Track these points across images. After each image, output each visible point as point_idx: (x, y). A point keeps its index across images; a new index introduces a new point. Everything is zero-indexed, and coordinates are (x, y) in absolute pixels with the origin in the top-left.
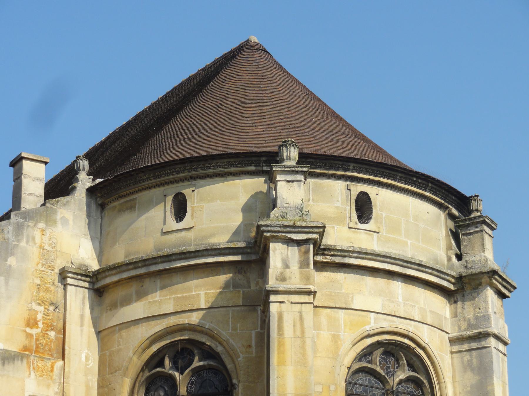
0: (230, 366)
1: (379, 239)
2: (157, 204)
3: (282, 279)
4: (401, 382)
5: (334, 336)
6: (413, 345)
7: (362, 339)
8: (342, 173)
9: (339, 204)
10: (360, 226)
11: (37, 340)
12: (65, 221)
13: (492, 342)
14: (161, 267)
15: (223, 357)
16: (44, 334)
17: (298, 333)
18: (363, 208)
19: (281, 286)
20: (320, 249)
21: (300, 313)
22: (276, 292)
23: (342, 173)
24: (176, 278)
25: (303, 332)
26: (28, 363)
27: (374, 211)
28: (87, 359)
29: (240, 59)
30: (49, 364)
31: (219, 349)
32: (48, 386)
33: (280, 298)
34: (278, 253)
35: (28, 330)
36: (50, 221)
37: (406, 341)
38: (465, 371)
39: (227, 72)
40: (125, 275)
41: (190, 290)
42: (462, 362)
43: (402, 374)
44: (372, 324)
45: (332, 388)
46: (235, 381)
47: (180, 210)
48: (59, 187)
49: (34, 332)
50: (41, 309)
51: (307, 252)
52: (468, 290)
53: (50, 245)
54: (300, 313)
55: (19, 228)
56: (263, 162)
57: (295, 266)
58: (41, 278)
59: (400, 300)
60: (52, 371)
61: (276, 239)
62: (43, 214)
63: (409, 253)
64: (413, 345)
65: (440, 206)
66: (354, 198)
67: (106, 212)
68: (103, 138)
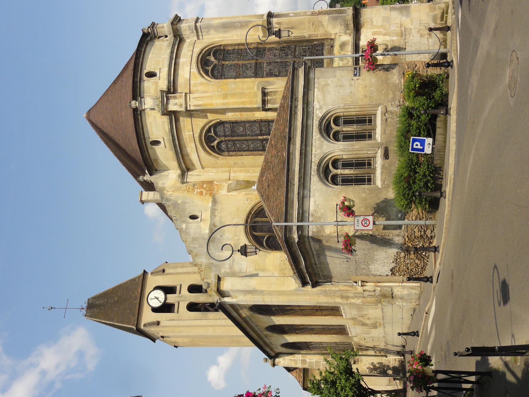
2: (326, 259)
3: (181, 105)
4: (215, 59)
6: (201, 55)
9: (151, 84)
10: (158, 76)
12: (163, 184)
13: (198, 24)
14: (178, 148)
16: (205, 189)
17: (201, 99)
18: (151, 75)
19: (184, 106)
20: (169, 92)
21: (193, 98)
22: (186, 107)
24: (182, 143)
25: (200, 97)
28: (213, 173)
29: (94, 120)
30: (216, 186)
32: (224, 186)
33: (188, 106)
34: (172, 107)
35: (204, 194)
38: (209, 34)
39: (99, 125)
40: (182, 161)
41: (186, 138)
43: (212, 58)
47: (156, 143)
48: (149, 187)
49: (204, 192)
51: (171, 96)
52: (179, 33)
54: (193, 98)
55: (167, 200)
56: (138, 115)
57: (176, 101)
62: (161, 191)
64: (201, 55)
65: (147, 44)
67: (158, 169)
68: (125, 168)
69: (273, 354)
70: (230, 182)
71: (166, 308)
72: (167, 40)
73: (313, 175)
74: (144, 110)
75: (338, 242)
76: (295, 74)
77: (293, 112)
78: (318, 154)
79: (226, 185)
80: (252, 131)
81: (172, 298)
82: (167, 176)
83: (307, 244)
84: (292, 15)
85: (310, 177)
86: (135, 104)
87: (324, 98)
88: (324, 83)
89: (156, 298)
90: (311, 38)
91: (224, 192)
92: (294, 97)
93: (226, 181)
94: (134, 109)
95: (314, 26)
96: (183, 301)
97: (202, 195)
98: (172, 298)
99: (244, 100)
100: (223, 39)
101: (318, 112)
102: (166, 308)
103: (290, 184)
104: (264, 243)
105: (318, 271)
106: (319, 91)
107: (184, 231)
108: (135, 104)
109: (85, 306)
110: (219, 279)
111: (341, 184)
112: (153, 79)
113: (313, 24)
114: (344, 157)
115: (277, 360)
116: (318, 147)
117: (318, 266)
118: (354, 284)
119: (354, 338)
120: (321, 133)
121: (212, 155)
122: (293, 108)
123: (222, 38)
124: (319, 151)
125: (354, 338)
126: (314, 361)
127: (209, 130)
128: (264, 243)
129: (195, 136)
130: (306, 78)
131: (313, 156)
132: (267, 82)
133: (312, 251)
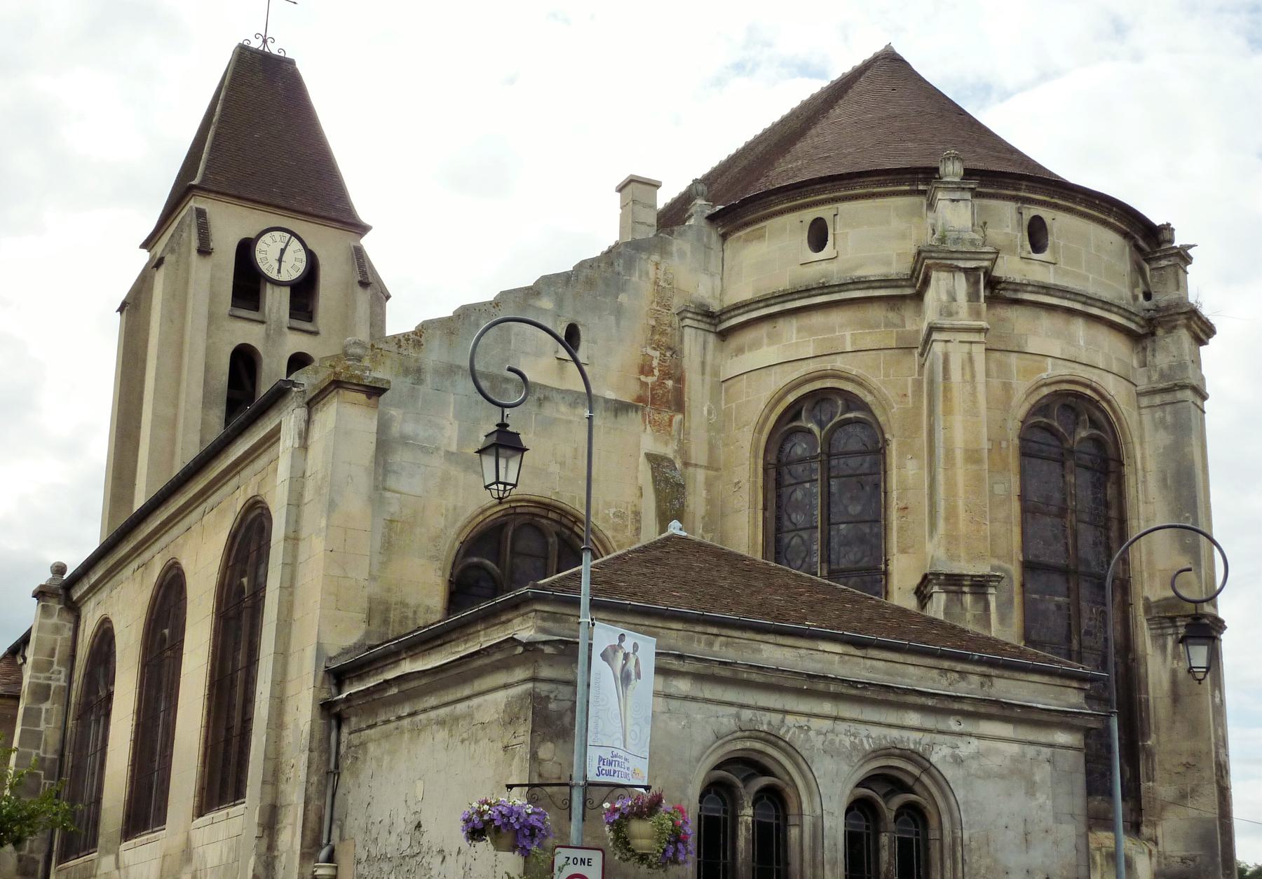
0: (881, 419)
1: (1056, 272)
4: (1082, 439)
5: (1004, 384)
7: (1037, 388)
8: (1014, 193)
9: (1009, 230)
11: (653, 389)
12: (682, 254)
15: (873, 408)
16: (661, 384)
17: (968, 377)
18: (1037, 235)
20: (993, 283)
21: (970, 354)
23: (1014, 193)
25: (973, 376)
26: (644, 416)
27: (1050, 238)
28: (709, 413)
31: (868, 399)
32: (666, 444)
33: (944, 336)
35: (643, 378)
36: (664, 252)
37: (1088, 392)
38: (1156, 430)
42: (1153, 419)
44: (1050, 371)
45: (1004, 445)
46: (887, 436)
47: (818, 236)
49: (650, 380)
50: (657, 354)
51: (977, 282)
53: (666, 281)
54: (970, 354)
58: (657, 319)
59: (1082, 343)
60: (670, 425)
61: (940, 267)
63: (1091, 289)
64: (1097, 398)
65: (1125, 235)
66: (1026, 223)
69: (76, 594)
70: (678, 465)
71: (248, 284)
72: (1135, 298)
73: (738, 717)
74: (931, 206)
75: (510, 787)
76: (1068, 683)
77: (946, 664)
78: (808, 740)
79: (669, 450)
80: (846, 543)
81: (277, 302)
82: (706, 270)
83: (501, 678)
84: (1217, 700)
85: (731, 704)
86: (954, 175)
87: (988, 775)
88: (1037, 778)
89: (280, 258)
90: (1142, 758)
91: (650, 442)
92: (993, 672)
93: (683, 451)
94: (937, 170)
95: (1181, 769)
96: (268, 335)
97: (642, 372)
98: (277, 302)
99: (962, 515)
100: (1140, 473)
101: (946, 751)
102: (248, 284)
103: (715, 630)
104: (475, 560)
105: (387, 722)
106: (1014, 760)
107: (531, 302)
108: (954, 175)
109: (273, 49)
110: (375, 392)
111: (703, 814)
112: (1022, 239)
113: (1188, 766)
114: (794, 833)
115: (56, 606)
116: (832, 742)
117: (406, 722)
118: (324, 853)
119: (112, 858)
120: (878, 753)
121: (771, 411)
122: (960, 666)
123: (1144, 469)
124: (818, 742)
125: (112, 858)
126: (43, 726)
127: (852, 401)
128: (475, 560)
129: (839, 358)
130: (1055, 719)
131: (803, 721)
132: (1011, 601)
133: (468, 698)
